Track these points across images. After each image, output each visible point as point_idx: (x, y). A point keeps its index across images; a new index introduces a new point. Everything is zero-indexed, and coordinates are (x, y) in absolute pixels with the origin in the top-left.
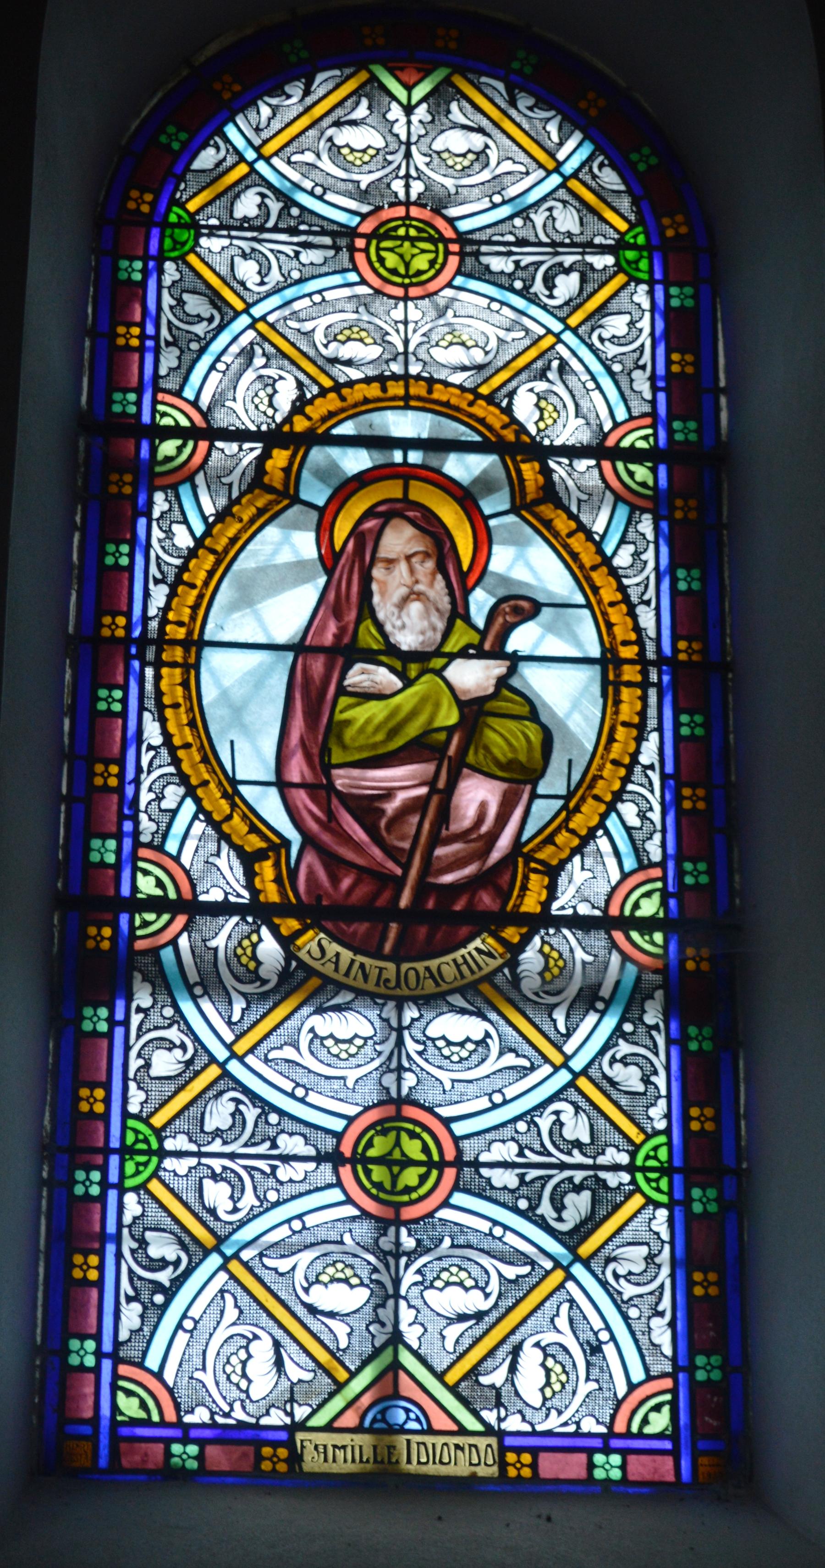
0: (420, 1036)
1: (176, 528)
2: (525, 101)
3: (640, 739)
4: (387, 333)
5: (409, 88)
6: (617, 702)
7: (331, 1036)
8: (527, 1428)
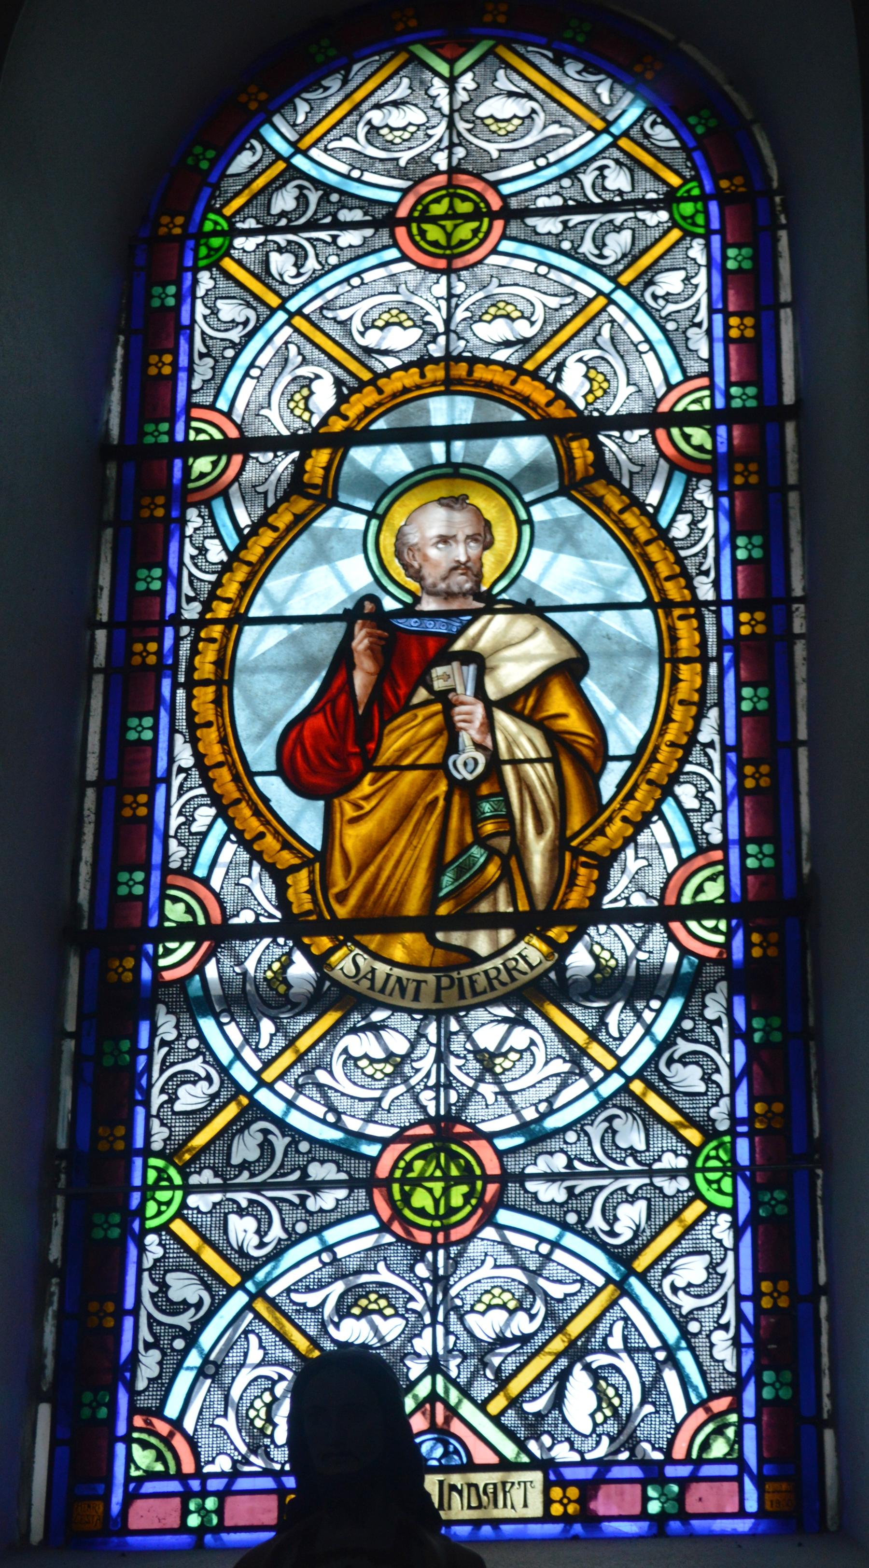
0: (469, 117)
1: (209, 543)
2: (572, 68)
3: (698, 718)
4: (427, 314)
5: (451, 62)
6: (675, 680)
7: (366, 1056)
8: (576, 1457)
